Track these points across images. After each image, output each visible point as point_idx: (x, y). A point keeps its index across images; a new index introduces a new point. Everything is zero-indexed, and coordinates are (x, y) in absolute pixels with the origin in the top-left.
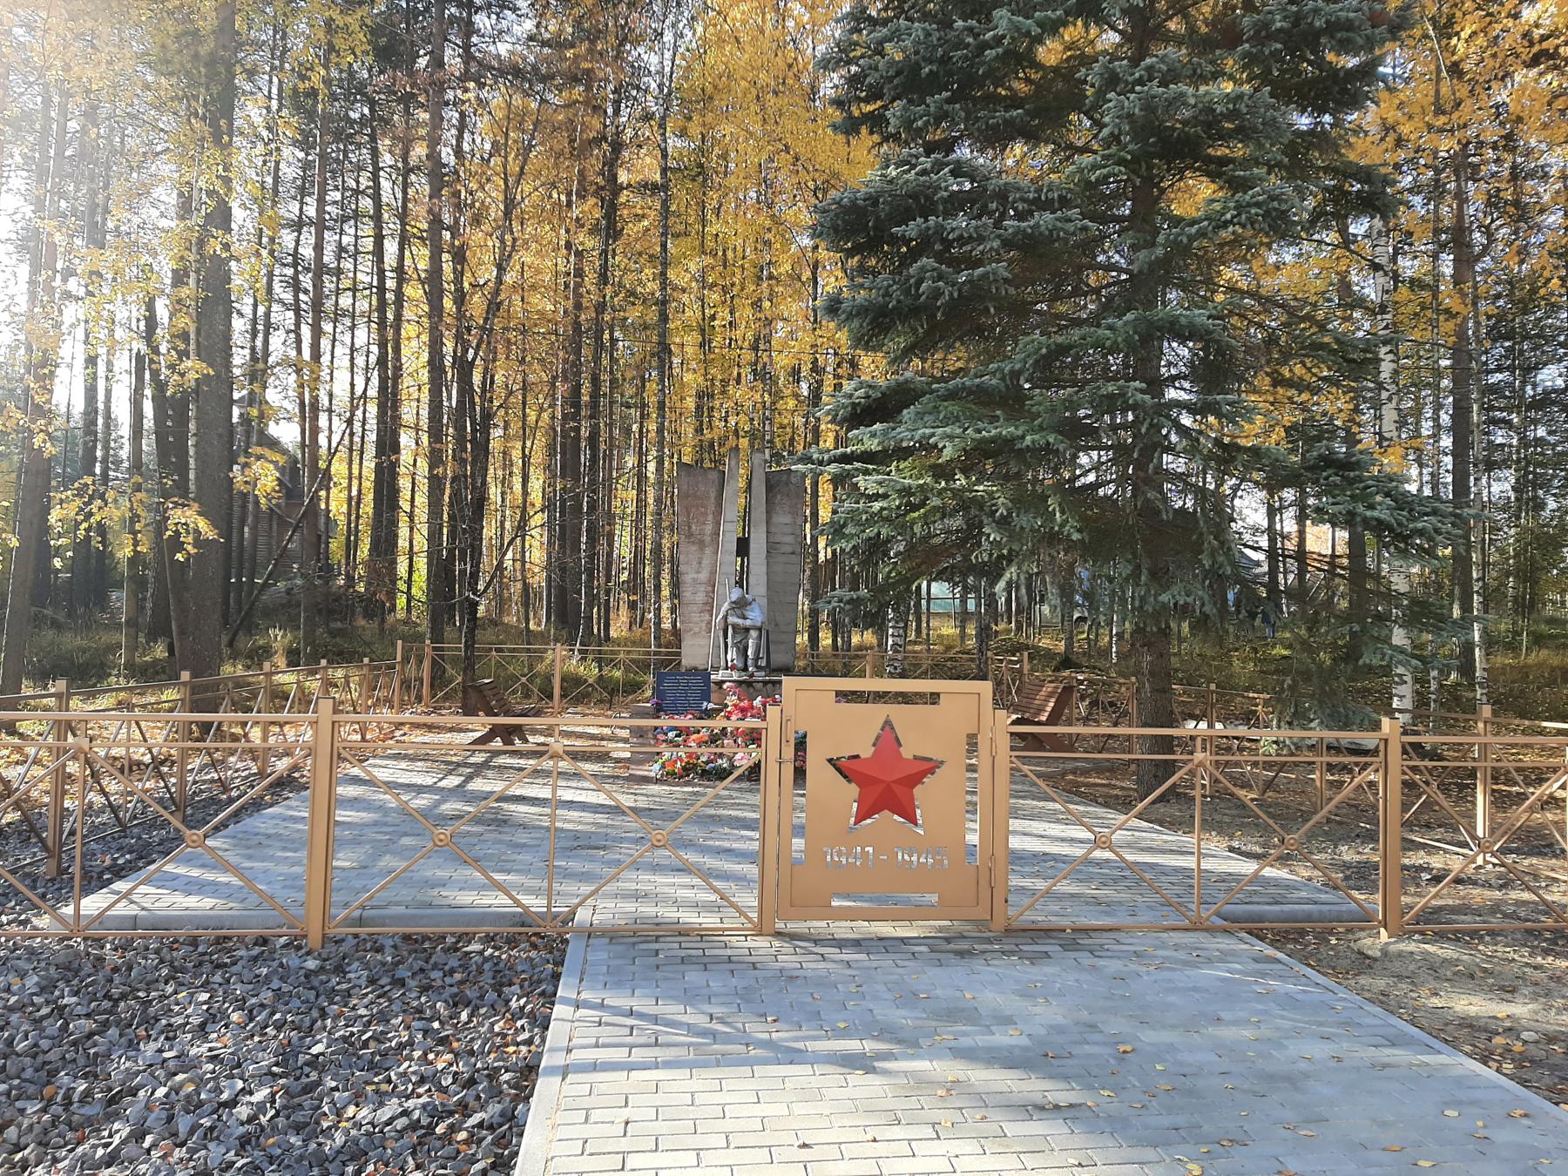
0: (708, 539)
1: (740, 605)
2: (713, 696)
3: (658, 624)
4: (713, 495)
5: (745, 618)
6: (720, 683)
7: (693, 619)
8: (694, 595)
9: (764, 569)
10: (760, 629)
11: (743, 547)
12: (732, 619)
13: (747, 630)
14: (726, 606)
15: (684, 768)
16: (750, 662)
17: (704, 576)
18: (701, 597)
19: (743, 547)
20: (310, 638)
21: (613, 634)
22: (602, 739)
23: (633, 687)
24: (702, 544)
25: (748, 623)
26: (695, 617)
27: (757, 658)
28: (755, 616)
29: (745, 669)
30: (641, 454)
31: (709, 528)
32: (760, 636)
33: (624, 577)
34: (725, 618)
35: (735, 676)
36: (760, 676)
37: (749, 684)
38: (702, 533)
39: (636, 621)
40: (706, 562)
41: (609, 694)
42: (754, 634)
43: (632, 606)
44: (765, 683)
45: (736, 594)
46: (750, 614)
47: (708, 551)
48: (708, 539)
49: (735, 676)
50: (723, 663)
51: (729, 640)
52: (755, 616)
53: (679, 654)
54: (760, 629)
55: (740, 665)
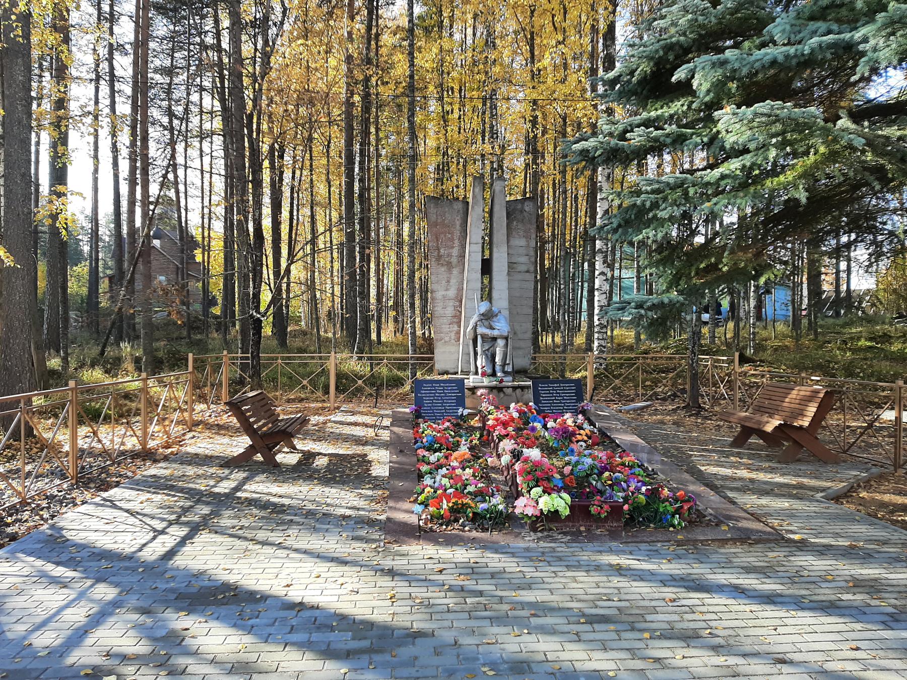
0: (454, 260)
1: (488, 317)
2: (468, 402)
3: (414, 333)
4: (458, 223)
5: (492, 328)
6: (473, 390)
7: (442, 331)
8: (442, 309)
9: (506, 284)
10: (506, 338)
11: (487, 267)
12: (480, 330)
13: (494, 339)
14: (475, 318)
15: (452, 510)
16: (498, 368)
17: (452, 293)
18: (450, 311)
19: (487, 267)
20: (149, 351)
21: (383, 339)
22: (366, 443)
23: (397, 382)
24: (449, 265)
25: (496, 333)
26: (446, 328)
27: (504, 364)
28: (501, 326)
29: (494, 374)
30: (399, 223)
31: (455, 252)
32: (507, 344)
33: (391, 303)
34: (475, 328)
35: (486, 381)
36: (508, 381)
37: (500, 389)
38: (450, 255)
39: (400, 329)
40: (453, 281)
41: (378, 387)
42: (501, 342)
43: (396, 320)
44: (515, 388)
45: (484, 307)
46: (497, 325)
47: (455, 271)
48: (454, 260)
49: (486, 381)
50: (473, 369)
51: (479, 349)
52: (501, 326)
53: (431, 359)
54: (506, 338)
55: (489, 371)
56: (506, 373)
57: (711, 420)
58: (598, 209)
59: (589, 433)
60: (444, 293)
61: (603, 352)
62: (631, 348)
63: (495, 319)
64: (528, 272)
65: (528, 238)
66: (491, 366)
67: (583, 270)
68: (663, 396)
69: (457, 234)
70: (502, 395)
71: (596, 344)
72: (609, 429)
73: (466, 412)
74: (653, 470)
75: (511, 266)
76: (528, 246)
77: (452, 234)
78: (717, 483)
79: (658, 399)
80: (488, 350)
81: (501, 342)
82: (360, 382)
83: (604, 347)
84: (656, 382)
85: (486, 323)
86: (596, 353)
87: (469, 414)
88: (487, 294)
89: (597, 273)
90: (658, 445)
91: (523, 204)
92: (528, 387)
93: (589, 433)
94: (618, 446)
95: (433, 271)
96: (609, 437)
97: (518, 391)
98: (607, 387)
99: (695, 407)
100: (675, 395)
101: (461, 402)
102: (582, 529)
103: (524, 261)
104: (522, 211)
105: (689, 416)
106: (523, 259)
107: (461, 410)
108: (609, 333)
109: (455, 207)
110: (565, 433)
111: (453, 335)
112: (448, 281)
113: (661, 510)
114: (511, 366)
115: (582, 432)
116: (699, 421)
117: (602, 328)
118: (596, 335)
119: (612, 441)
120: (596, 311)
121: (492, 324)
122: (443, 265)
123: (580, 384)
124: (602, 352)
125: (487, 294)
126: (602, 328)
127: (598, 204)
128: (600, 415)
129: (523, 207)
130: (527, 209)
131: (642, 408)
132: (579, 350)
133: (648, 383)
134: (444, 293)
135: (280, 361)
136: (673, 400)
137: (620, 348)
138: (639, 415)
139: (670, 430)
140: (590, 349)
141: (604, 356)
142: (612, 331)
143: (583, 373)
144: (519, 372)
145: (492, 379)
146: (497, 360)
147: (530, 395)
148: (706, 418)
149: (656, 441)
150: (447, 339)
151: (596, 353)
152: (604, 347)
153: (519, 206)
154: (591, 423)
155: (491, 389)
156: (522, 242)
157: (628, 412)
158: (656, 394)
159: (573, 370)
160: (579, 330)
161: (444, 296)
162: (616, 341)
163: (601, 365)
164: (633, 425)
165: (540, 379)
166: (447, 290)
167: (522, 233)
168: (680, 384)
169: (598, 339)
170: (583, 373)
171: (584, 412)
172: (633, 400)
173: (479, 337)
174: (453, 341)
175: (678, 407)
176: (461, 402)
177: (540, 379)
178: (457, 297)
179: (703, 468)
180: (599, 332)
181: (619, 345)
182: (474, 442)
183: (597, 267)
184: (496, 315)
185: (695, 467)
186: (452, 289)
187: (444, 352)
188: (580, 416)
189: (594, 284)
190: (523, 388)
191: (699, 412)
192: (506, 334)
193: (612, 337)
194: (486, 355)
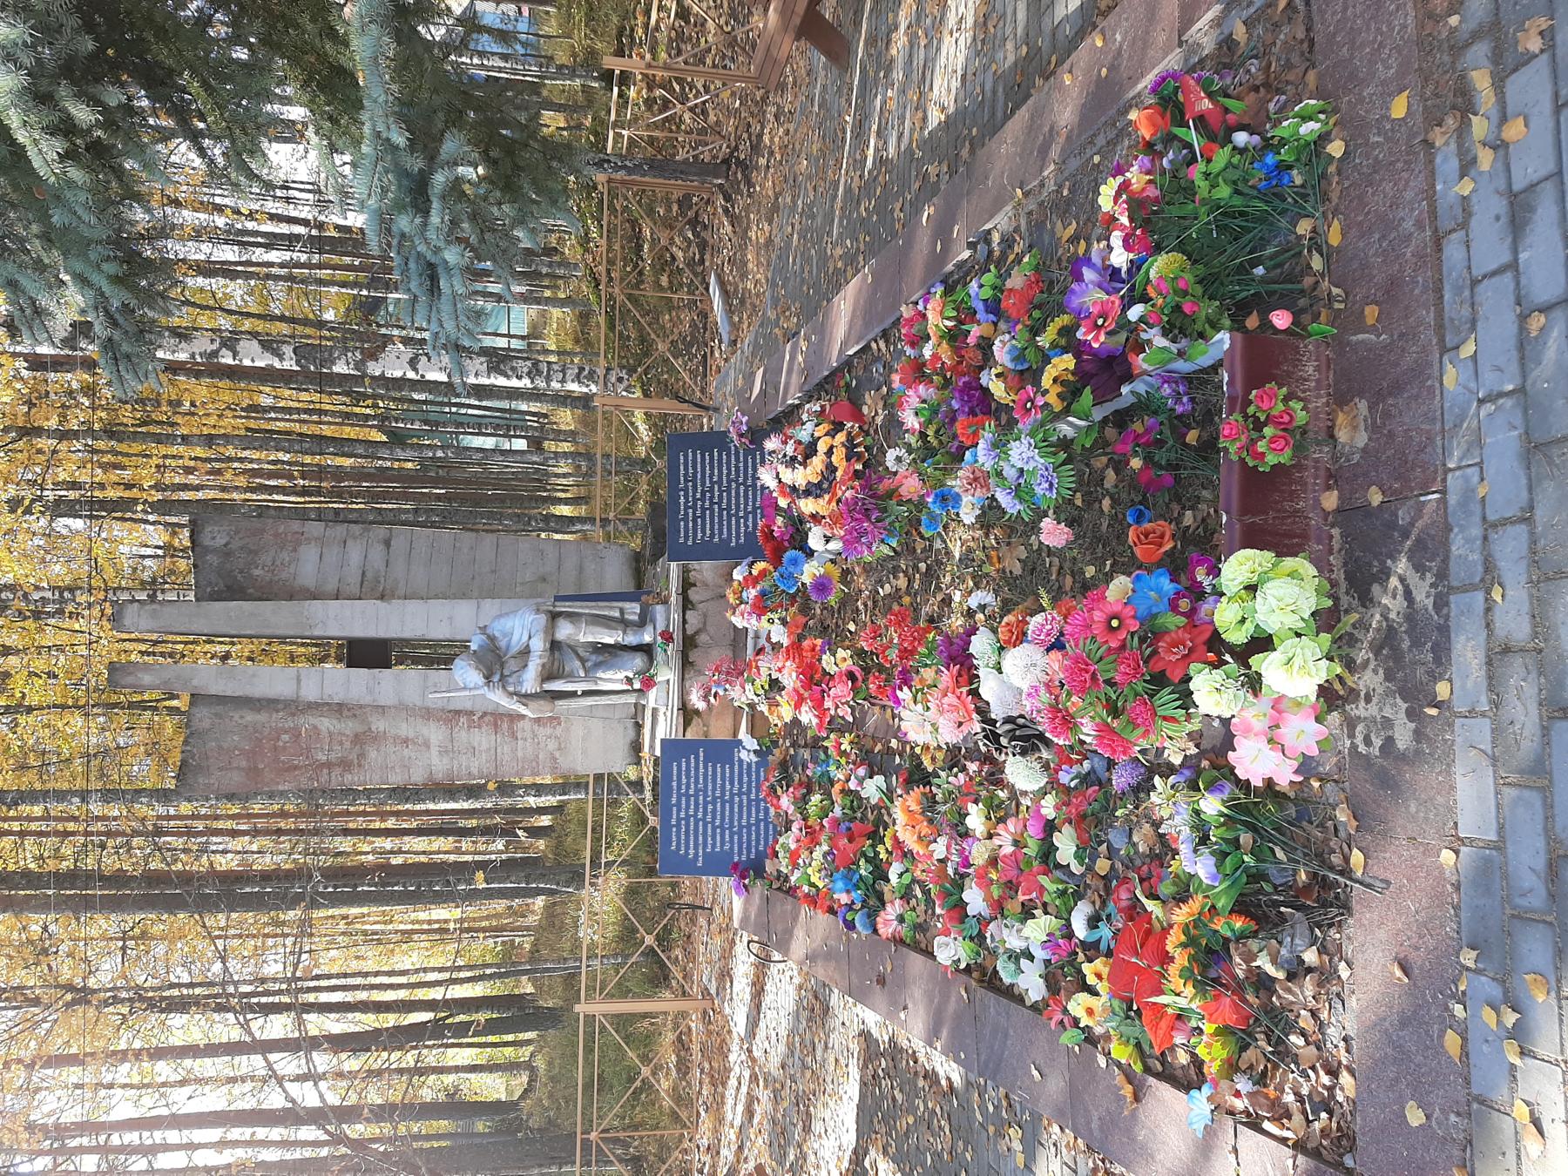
0: (349, 727)
1: (496, 662)
2: (719, 731)
4: (250, 717)
5: (526, 652)
6: (688, 714)
9: (413, 605)
10: (554, 616)
11: (368, 654)
12: (530, 680)
13: (555, 646)
16: (631, 639)
17: (435, 733)
18: (482, 739)
19: (368, 654)
25: (538, 645)
26: (524, 749)
27: (624, 623)
28: (521, 627)
29: (646, 650)
31: (326, 724)
32: (570, 616)
34: (525, 698)
35: (667, 674)
36: (667, 616)
37: (689, 643)
40: (405, 730)
42: (565, 631)
44: (687, 604)
47: (379, 725)
49: (667, 674)
51: (580, 687)
54: (554, 616)
55: (639, 661)
56: (644, 620)
57: (760, 136)
58: (260, 364)
59: (824, 428)
60: (434, 751)
61: (592, 374)
62: (584, 317)
63: (503, 644)
64: (387, 543)
65: (298, 541)
66: (626, 656)
67: (425, 402)
68: (694, 249)
69: (277, 719)
70: (703, 638)
71: (573, 387)
72: (807, 371)
73: (750, 743)
74: (972, 246)
75: (375, 589)
76: (321, 541)
77: (279, 732)
78: (1009, 55)
79: (702, 261)
80: (583, 661)
81: (565, 631)
82: (649, 940)
83: (581, 369)
84: (664, 262)
85: (512, 665)
86: (594, 388)
87: (752, 731)
88: (438, 655)
89: (411, 375)
90: (839, 251)
91: (207, 550)
92: (685, 571)
93: (824, 428)
94: (866, 349)
95: (376, 778)
96: (834, 373)
97: (693, 595)
98: (672, 370)
99: (733, 169)
100: (694, 223)
101: (723, 751)
102: (1330, 500)
103: (359, 553)
104: (226, 552)
105: (750, 184)
106: (355, 553)
107: (744, 755)
108: (553, 358)
109: (206, 724)
110: (866, 513)
111: (543, 732)
112: (406, 741)
113: (1224, 192)
114: (627, 605)
115: (822, 447)
116: (762, 161)
117: (539, 373)
118: (555, 385)
119: (847, 364)
120: (501, 381)
121: (514, 650)
122: (362, 756)
123: (673, 441)
124: (591, 376)
125: (438, 655)
126: (539, 373)
127: (247, 362)
128: (763, 392)
129: (215, 550)
130: (220, 541)
131: (725, 294)
132: (588, 424)
133: (664, 280)
134: (434, 751)
135: (593, 1136)
136: (705, 227)
137: (583, 339)
138: (742, 302)
139: (788, 228)
140: (585, 401)
141: (600, 372)
142: (547, 352)
143: (639, 417)
144: (641, 586)
145: (659, 656)
146: (611, 641)
147: (705, 570)
148: (756, 148)
149: (824, 258)
150: (552, 745)
151: (594, 388)
152: (581, 369)
153: (212, 559)
154: (790, 416)
155: (686, 664)
156: (309, 554)
157: (735, 327)
158: (691, 263)
159: (631, 437)
160: (545, 416)
161: (444, 752)
162: (569, 346)
163: (620, 380)
164: (771, 314)
165: (660, 537)
166: (427, 744)
167: (285, 556)
168: (669, 209)
169: (563, 381)
170: (639, 417)
171: (756, 436)
172: (704, 315)
173: (547, 687)
174: (558, 731)
175: (726, 211)
176: (723, 751)
177: (660, 537)
178: (448, 721)
179: (935, 117)
180: (548, 379)
181: (577, 341)
182: (845, 746)
183: (398, 374)
184: (492, 639)
185: (931, 146)
186: (425, 731)
187: (584, 752)
188: (771, 444)
189: (435, 382)
190: (686, 585)
191: (739, 163)
192: (542, 619)
193: (559, 353)
194: (597, 665)
